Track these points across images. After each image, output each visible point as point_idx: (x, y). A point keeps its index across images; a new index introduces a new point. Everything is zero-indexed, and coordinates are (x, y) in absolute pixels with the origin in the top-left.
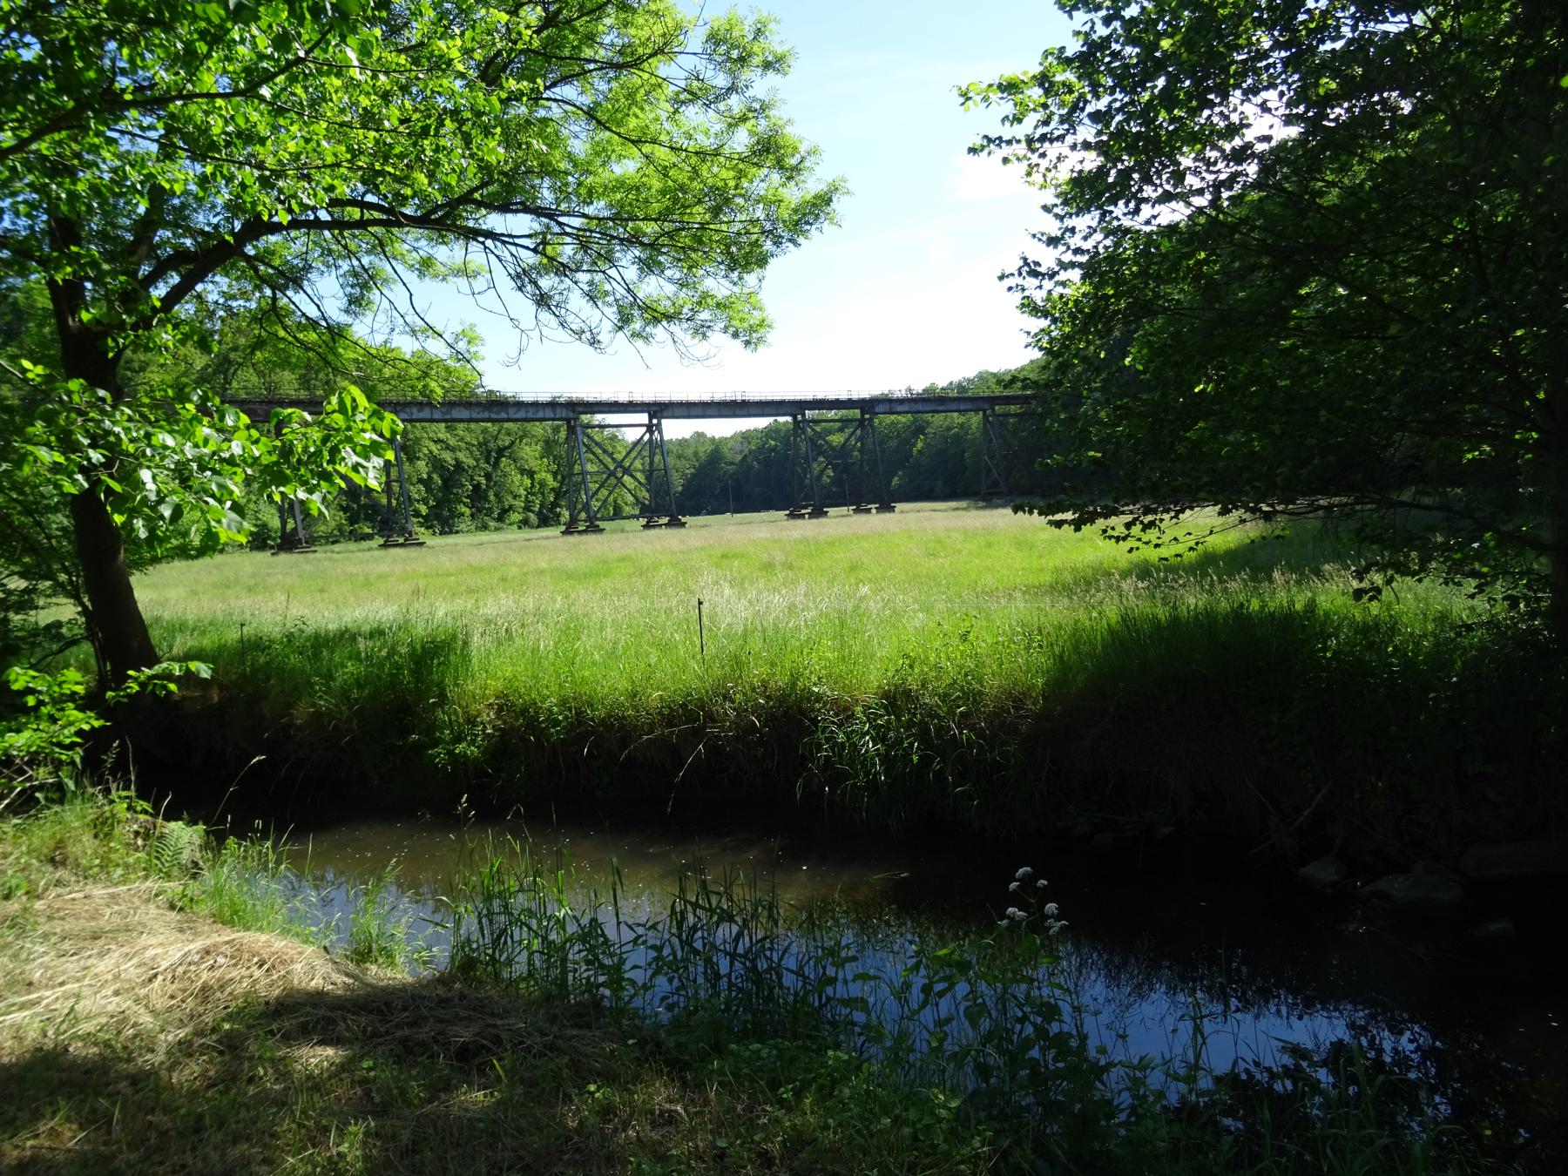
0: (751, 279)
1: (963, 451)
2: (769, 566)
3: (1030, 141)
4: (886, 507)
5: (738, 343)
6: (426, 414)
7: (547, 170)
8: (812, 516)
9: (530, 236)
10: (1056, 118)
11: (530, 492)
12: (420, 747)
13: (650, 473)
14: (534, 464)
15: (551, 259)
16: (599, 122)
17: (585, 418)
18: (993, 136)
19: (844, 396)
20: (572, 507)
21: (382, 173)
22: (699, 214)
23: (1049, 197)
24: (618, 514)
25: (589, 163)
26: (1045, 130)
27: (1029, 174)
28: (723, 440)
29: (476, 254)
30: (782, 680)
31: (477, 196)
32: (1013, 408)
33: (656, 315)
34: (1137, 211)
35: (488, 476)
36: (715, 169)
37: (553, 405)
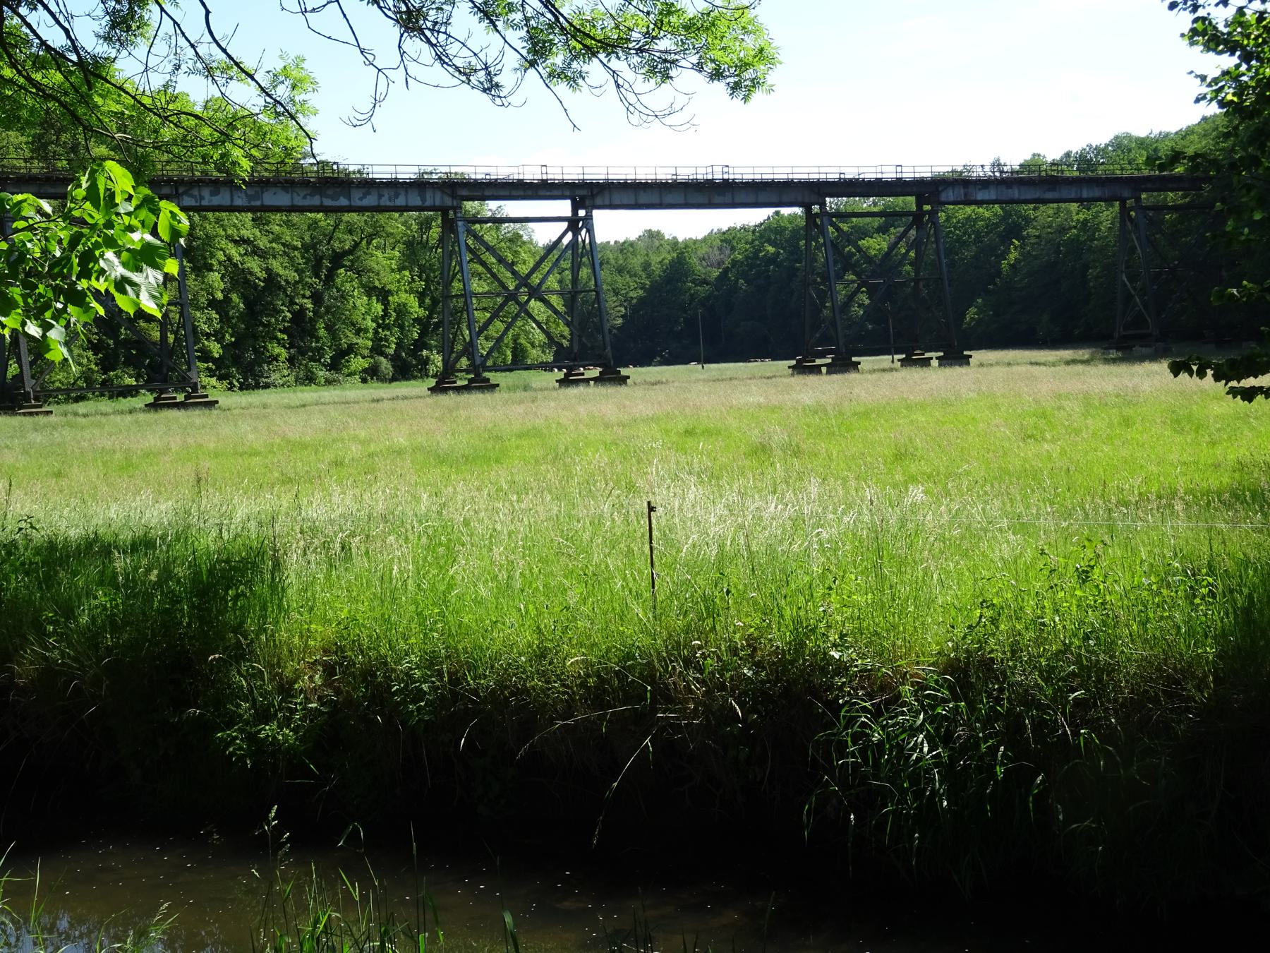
2: (762, 451)
4: (955, 357)
5: (720, 87)
6: (223, 198)
8: (832, 369)
11: (381, 323)
13: (571, 296)
14: (388, 279)
17: (471, 206)
19: (889, 174)
20: (446, 349)
24: (519, 362)
28: (691, 245)
32: (1171, 197)
35: (317, 298)
37: (420, 185)
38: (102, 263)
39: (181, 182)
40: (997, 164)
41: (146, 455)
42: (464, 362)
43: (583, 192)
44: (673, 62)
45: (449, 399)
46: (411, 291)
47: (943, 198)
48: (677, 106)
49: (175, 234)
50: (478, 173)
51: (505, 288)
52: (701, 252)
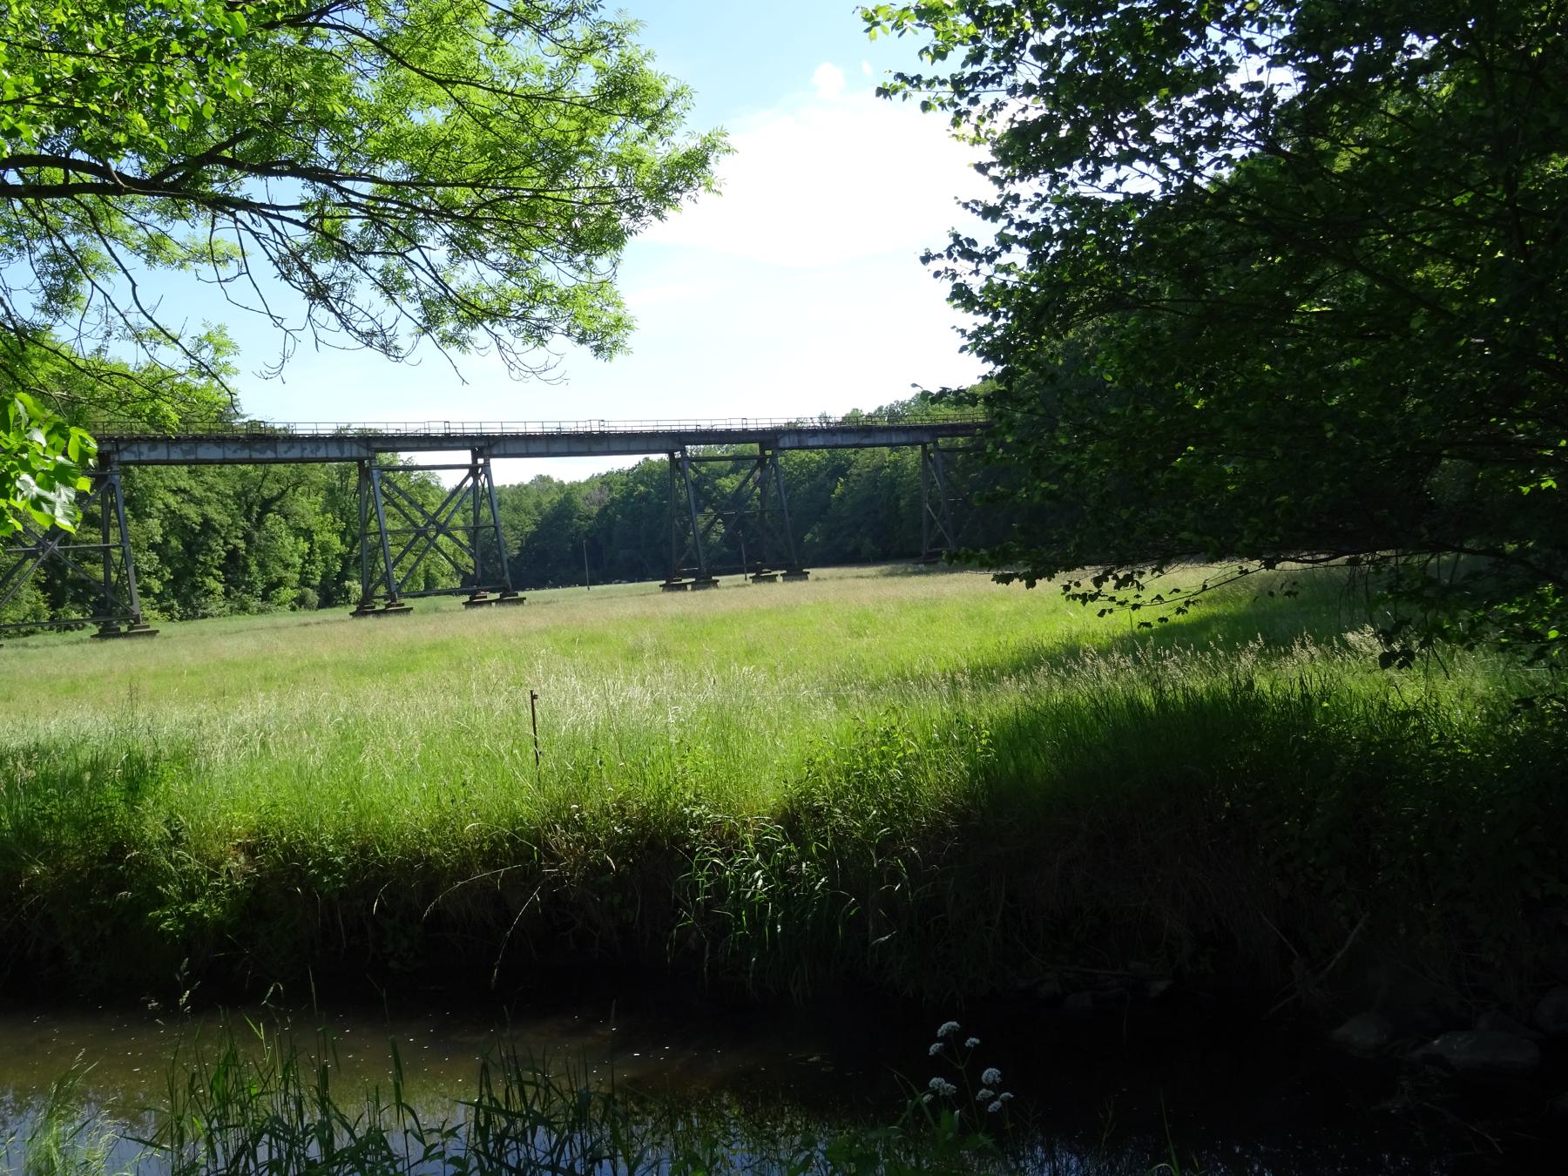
0: (602, 264)
1: (898, 498)
2: (634, 654)
3: (958, 84)
4: (795, 572)
5: (585, 349)
6: (161, 453)
7: (322, 120)
8: (695, 586)
9: (301, 207)
10: (990, 53)
11: (308, 559)
12: (138, 908)
13: (474, 532)
14: (313, 521)
15: (329, 237)
16: (394, 56)
17: (385, 458)
18: (910, 74)
19: (737, 426)
20: (367, 581)
21: (83, 113)
22: (532, 178)
23: (985, 154)
24: (430, 589)
25: (380, 110)
26: (976, 68)
27: (956, 123)
28: (575, 487)
29: (226, 233)
30: (647, 795)
31: (227, 153)
32: (961, 441)
33: (474, 313)
34: (1096, 175)
35: (248, 538)
36: (553, 119)
37: (339, 439)
38: (18, 484)
39: (121, 440)
40: (824, 417)
41: (91, 678)
42: (382, 590)
43: (482, 444)
44: (546, 328)
45: (369, 622)
46: (333, 531)
47: (781, 444)
48: (551, 364)
49: (84, 455)
50: (390, 430)
51: (414, 524)
52: (584, 493)
